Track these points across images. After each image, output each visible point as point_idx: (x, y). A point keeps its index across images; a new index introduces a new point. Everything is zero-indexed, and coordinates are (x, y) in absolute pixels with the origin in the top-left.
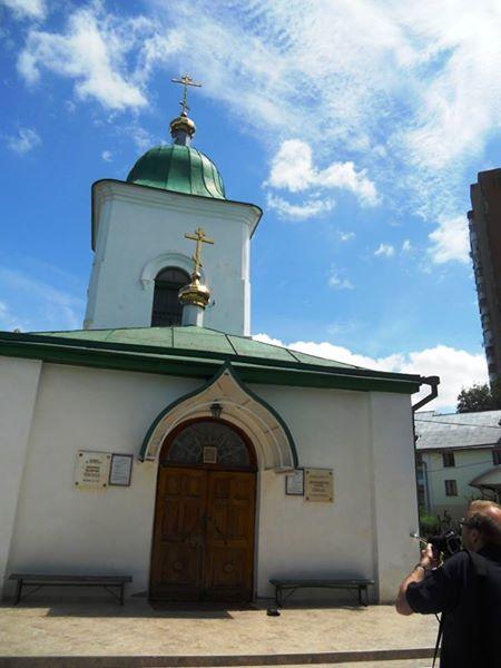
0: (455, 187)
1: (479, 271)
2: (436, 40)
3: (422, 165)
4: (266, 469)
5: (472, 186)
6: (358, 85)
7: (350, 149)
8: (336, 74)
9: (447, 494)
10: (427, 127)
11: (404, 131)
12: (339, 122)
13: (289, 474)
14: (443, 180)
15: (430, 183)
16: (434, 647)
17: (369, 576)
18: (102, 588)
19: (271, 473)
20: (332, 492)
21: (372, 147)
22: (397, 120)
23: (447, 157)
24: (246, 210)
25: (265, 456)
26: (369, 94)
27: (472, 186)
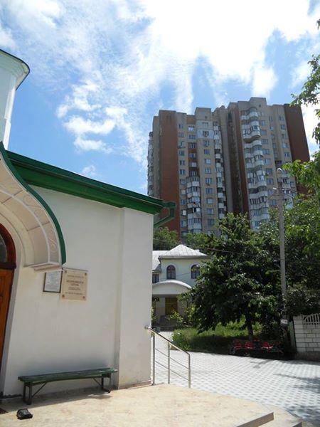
0: (139, 112)
1: (151, 169)
2: (143, 10)
3: (123, 91)
4: (25, 266)
5: (155, 117)
6: (89, 22)
7: (78, 66)
8: (75, 8)
9: (192, 278)
10: (127, 68)
11: (114, 66)
12: (73, 44)
13: (47, 271)
14: (133, 105)
15: (125, 105)
16: (22, 393)
17: (110, 365)
18: (93, 379)
19: (29, 269)
20: (86, 292)
21: (93, 69)
22: (111, 56)
23: (138, 90)
24: (18, 63)
25: (25, 250)
26: (95, 32)
27: (155, 117)
